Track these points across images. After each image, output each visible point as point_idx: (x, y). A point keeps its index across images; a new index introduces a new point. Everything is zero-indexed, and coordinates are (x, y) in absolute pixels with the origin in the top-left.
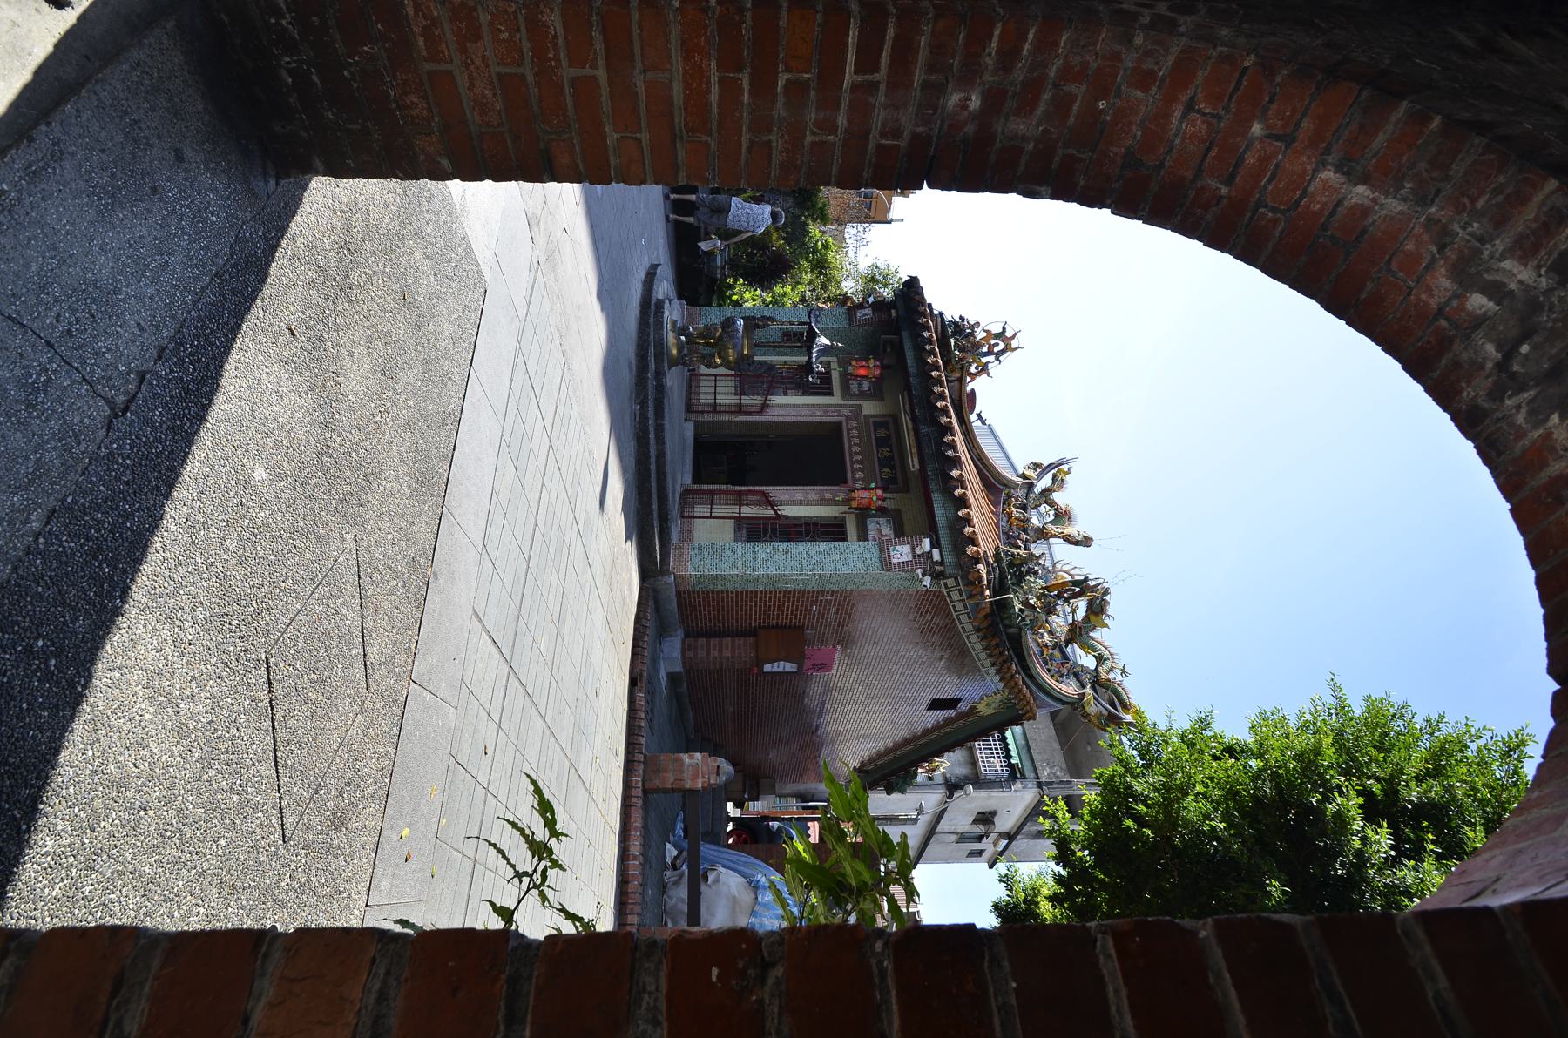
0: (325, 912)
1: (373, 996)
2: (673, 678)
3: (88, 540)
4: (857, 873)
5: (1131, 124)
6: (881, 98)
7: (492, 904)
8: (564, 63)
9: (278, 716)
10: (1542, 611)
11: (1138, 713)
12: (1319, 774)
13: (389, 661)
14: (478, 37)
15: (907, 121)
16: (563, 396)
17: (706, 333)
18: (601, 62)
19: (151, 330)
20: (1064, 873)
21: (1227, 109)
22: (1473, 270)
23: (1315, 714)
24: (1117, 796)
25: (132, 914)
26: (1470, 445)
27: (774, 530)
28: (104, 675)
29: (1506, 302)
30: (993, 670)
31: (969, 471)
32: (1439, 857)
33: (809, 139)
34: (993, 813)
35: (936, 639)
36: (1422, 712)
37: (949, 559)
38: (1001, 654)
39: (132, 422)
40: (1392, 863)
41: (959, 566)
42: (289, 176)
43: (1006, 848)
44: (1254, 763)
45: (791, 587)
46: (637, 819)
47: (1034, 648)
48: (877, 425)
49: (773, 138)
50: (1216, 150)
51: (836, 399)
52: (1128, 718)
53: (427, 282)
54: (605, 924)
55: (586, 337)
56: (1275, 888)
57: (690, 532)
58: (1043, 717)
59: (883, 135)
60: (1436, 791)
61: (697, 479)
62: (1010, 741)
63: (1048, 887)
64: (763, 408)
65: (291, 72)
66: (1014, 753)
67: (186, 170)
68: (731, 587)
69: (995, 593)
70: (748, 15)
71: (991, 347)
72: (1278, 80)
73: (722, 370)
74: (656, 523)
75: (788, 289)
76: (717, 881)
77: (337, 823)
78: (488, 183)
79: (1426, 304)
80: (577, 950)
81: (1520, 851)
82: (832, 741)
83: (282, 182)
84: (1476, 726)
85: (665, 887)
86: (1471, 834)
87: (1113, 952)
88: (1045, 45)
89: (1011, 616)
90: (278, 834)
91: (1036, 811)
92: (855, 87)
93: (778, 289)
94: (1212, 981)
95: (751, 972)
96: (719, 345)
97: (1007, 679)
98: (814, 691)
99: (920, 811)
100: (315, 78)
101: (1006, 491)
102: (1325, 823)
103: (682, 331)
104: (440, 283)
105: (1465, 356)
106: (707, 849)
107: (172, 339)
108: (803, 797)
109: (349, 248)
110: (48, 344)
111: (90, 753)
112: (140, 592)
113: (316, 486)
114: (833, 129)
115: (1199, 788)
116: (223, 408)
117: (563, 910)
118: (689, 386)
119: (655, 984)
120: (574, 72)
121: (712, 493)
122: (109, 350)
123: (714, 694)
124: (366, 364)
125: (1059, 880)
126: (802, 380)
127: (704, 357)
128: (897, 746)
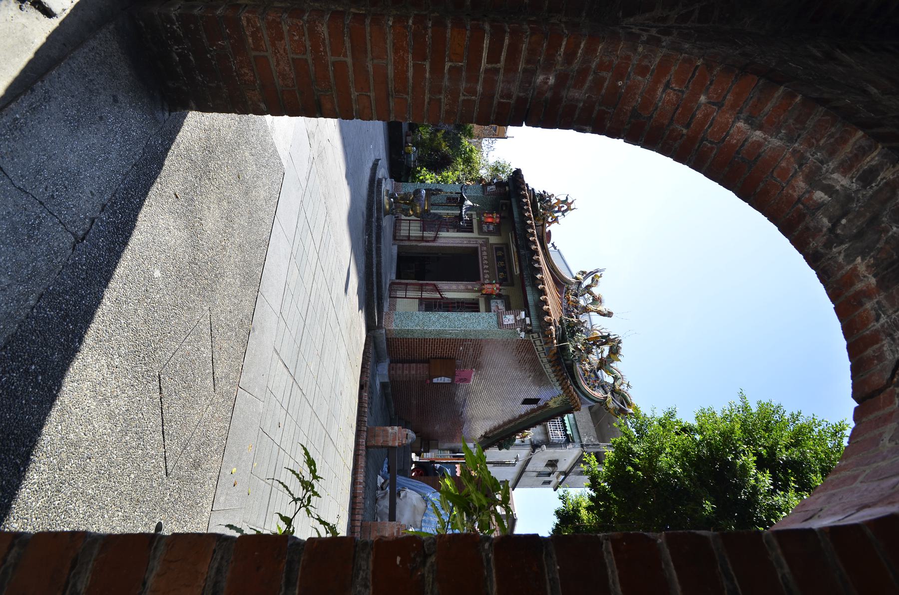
0: (189, 514)
1: (214, 571)
2: (383, 385)
3: (61, 310)
4: (479, 500)
5: (635, 94)
6: (501, 77)
7: (280, 515)
8: (329, 54)
9: (165, 407)
10: (849, 363)
11: (636, 408)
12: (733, 444)
13: (227, 376)
14: (282, 38)
15: (515, 90)
16: (326, 231)
17: (405, 197)
18: (349, 53)
19: (98, 195)
20: (594, 494)
21: (687, 87)
22: (817, 178)
23: (731, 411)
24: (624, 454)
25: (81, 516)
26: (814, 272)
27: (440, 305)
28: (68, 385)
29: (834, 196)
30: (557, 384)
31: (546, 275)
32: (797, 490)
33: (462, 98)
34: (557, 461)
35: (527, 366)
36: (789, 410)
37: (535, 323)
38: (562, 375)
39: (87, 245)
40: (772, 493)
41: (540, 327)
42: (176, 111)
43: (563, 480)
44: (698, 437)
45: (448, 336)
46: (362, 463)
47: (580, 372)
48: (497, 249)
49: (442, 97)
50: (680, 109)
51: (475, 235)
52: (631, 411)
53: (252, 168)
54: (342, 532)
55: (339, 199)
56: (708, 506)
57: (394, 305)
58: (584, 409)
59: (502, 97)
60: (796, 454)
61: (398, 276)
62: (566, 421)
63: (586, 502)
64: (436, 238)
65: (178, 54)
66: (568, 428)
67: (119, 107)
68: (416, 336)
69: (559, 342)
70: (430, 31)
71: (560, 208)
72: (715, 73)
73: (413, 218)
74: (375, 300)
75: (450, 174)
76: (405, 496)
77: (196, 465)
78: (286, 117)
79: (792, 195)
80: (326, 548)
81: (834, 495)
82: (470, 421)
83: (173, 114)
84: (818, 419)
85: (377, 499)
86: (814, 478)
87: (611, 550)
88: (590, 50)
89: (568, 354)
90: (163, 472)
91: (580, 460)
92: (487, 71)
93: (445, 174)
94: (663, 566)
95: (418, 559)
96: (412, 204)
97: (565, 389)
98: (460, 393)
99: (517, 459)
100: (192, 58)
101: (566, 286)
102: (736, 471)
103: (391, 196)
104: (259, 169)
105: (812, 224)
106: (400, 479)
107: (110, 200)
108: (453, 451)
109: (209, 150)
110: (41, 203)
111: (60, 427)
112: (89, 340)
113: (188, 280)
114: (474, 93)
115: (668, 450)
116: (137, 238)
117: (319, 519)
118: (395, 226)
119: (366, 565)
120: (333, 59)
121: (407, 284)
122: (74, 206)
123: (406, 394)
124: (217, 213)
125: (591, 498)
126: (456, 224)
127: (403, 210)
128: (505, 424)
